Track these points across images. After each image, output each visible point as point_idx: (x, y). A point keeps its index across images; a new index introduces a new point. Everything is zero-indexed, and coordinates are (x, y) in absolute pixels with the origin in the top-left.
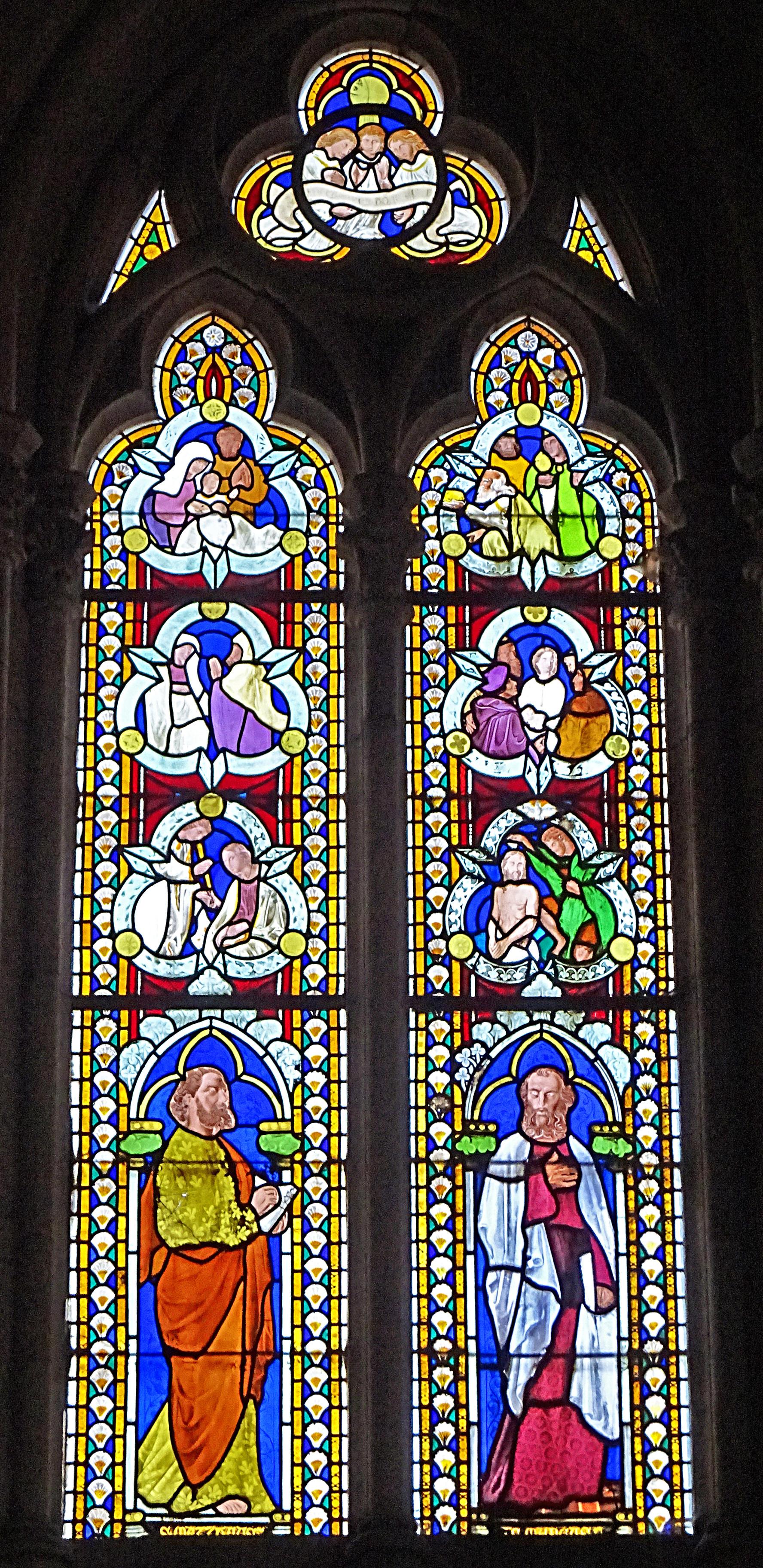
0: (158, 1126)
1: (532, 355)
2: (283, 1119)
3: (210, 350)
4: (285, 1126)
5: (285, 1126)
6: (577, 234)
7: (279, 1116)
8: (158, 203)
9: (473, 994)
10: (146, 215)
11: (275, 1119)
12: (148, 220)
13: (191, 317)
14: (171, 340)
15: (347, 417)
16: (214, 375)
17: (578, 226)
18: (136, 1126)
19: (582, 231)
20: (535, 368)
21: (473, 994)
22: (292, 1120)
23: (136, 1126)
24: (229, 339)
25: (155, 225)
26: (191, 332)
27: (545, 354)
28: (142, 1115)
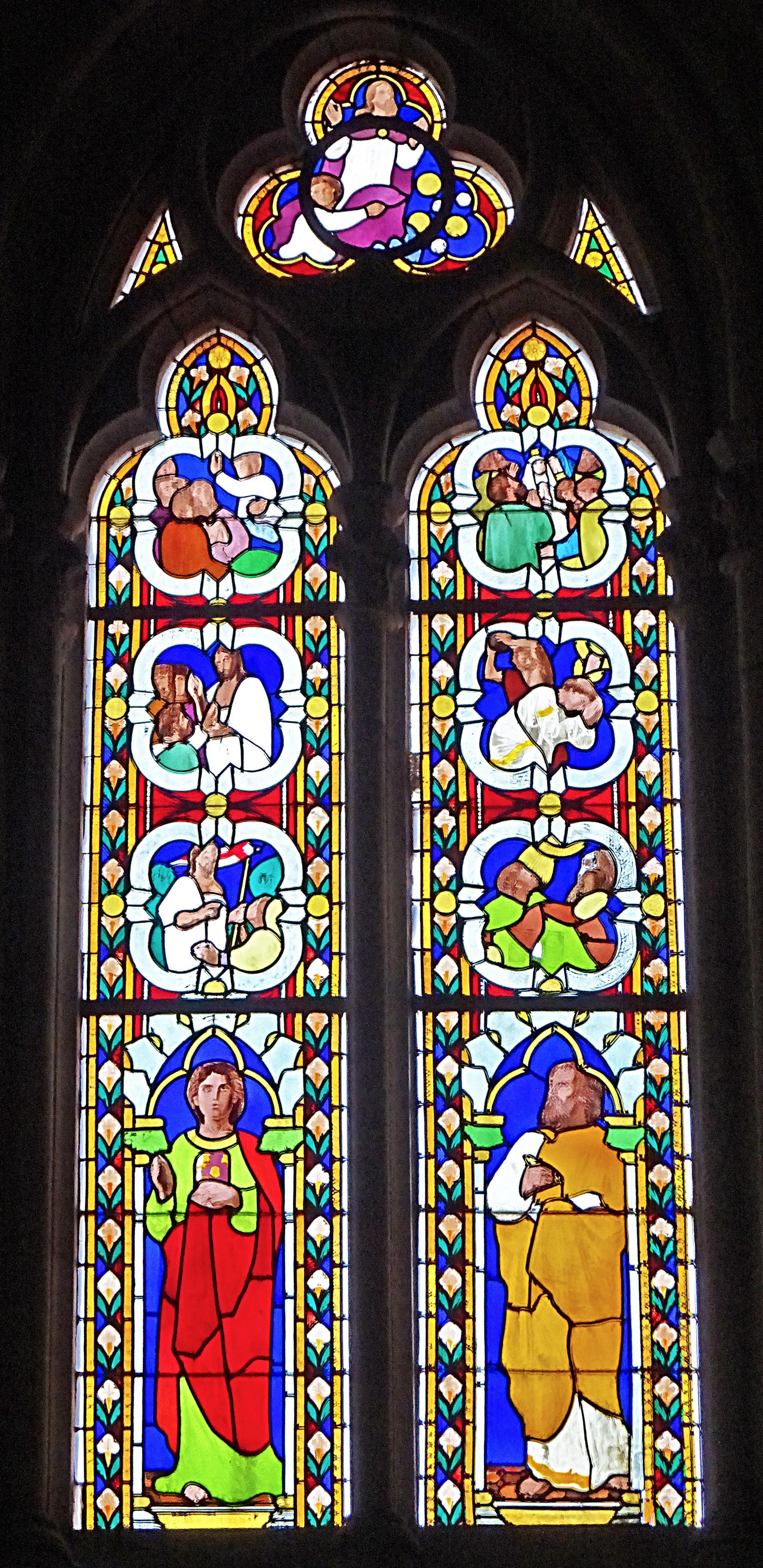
0: (159, 1122)
1: (540, 364)
2: (282, 1116)
3: (530, 365)
4: (289, 1123)
5: (289, 1123)
6: (586, 236)
7: (277, 1112)
8: (590, 208)
9: (146, 997)
10: (151, 237)
11: (274, 1116)
12: (153, 242)
13: (510, 331)
14: (174, 365)
15: (341, 436)
16: (538, 390)
17: (588, 228)
18: (140, 1123)
19: (592, 233)
20: (543, 378)
21: (146, 997)
22: (293, 1117)
23: (140, 1123)
24: (518, 354)
25: (161, 246)
26: (509, 349)
27: (554, 365)
28: (150, 1113)
